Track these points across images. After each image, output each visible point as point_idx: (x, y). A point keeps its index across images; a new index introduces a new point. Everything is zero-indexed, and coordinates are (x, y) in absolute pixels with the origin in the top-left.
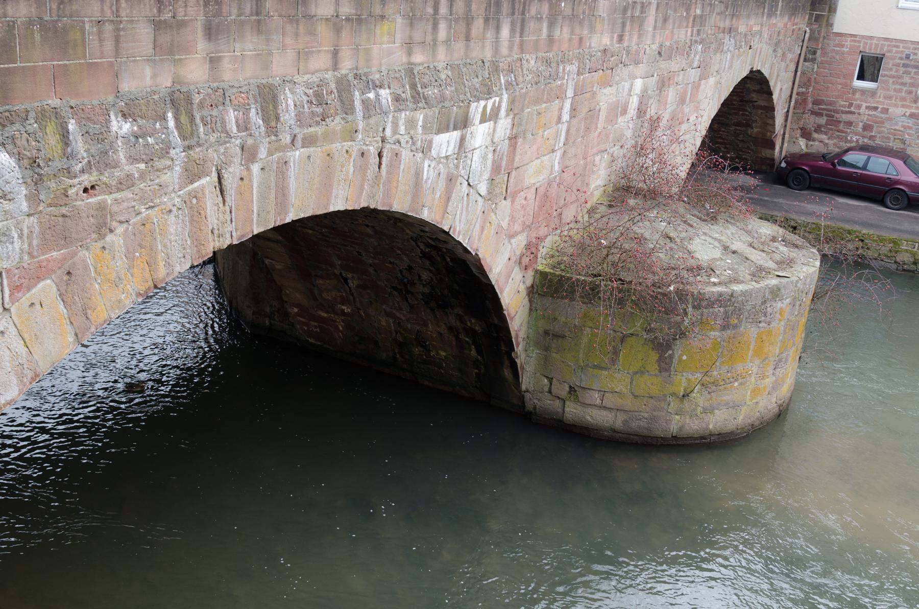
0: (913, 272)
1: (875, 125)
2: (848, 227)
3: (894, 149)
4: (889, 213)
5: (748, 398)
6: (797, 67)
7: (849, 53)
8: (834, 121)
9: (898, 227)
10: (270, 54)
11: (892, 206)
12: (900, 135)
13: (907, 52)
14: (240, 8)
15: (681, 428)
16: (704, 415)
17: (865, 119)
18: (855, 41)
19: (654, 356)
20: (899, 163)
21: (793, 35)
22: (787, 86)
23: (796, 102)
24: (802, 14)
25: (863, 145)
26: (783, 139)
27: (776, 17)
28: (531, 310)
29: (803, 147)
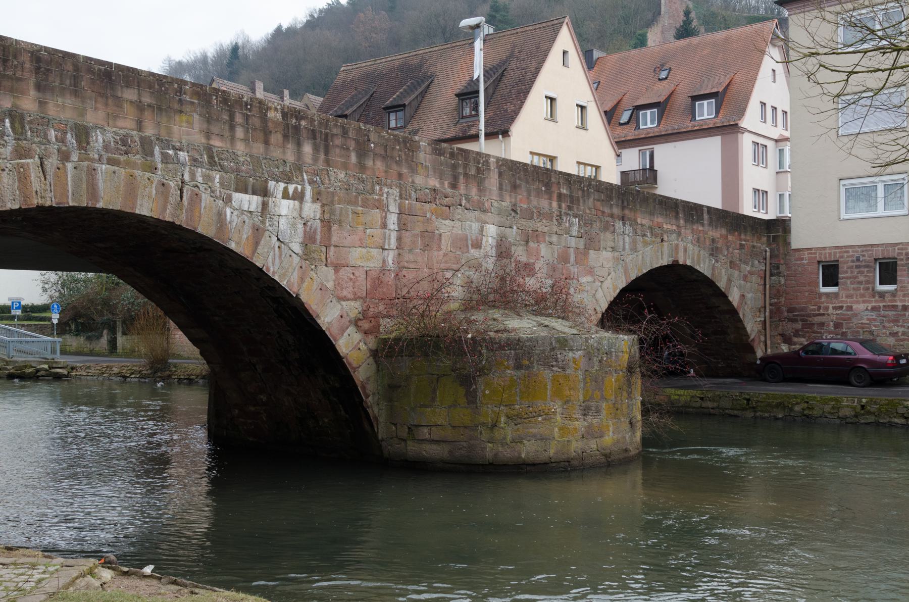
1: (844, 322)
6: (765, 282)
10: (85, 109)
12: (867, 328)
13: (856, 255)
14: (61, 80)
15: (496, 455)
16: (514, 444)
17: (834, 318)
18: (811, 253)
19: (462, 391)
23: (771, 311)
28: (378, 371)
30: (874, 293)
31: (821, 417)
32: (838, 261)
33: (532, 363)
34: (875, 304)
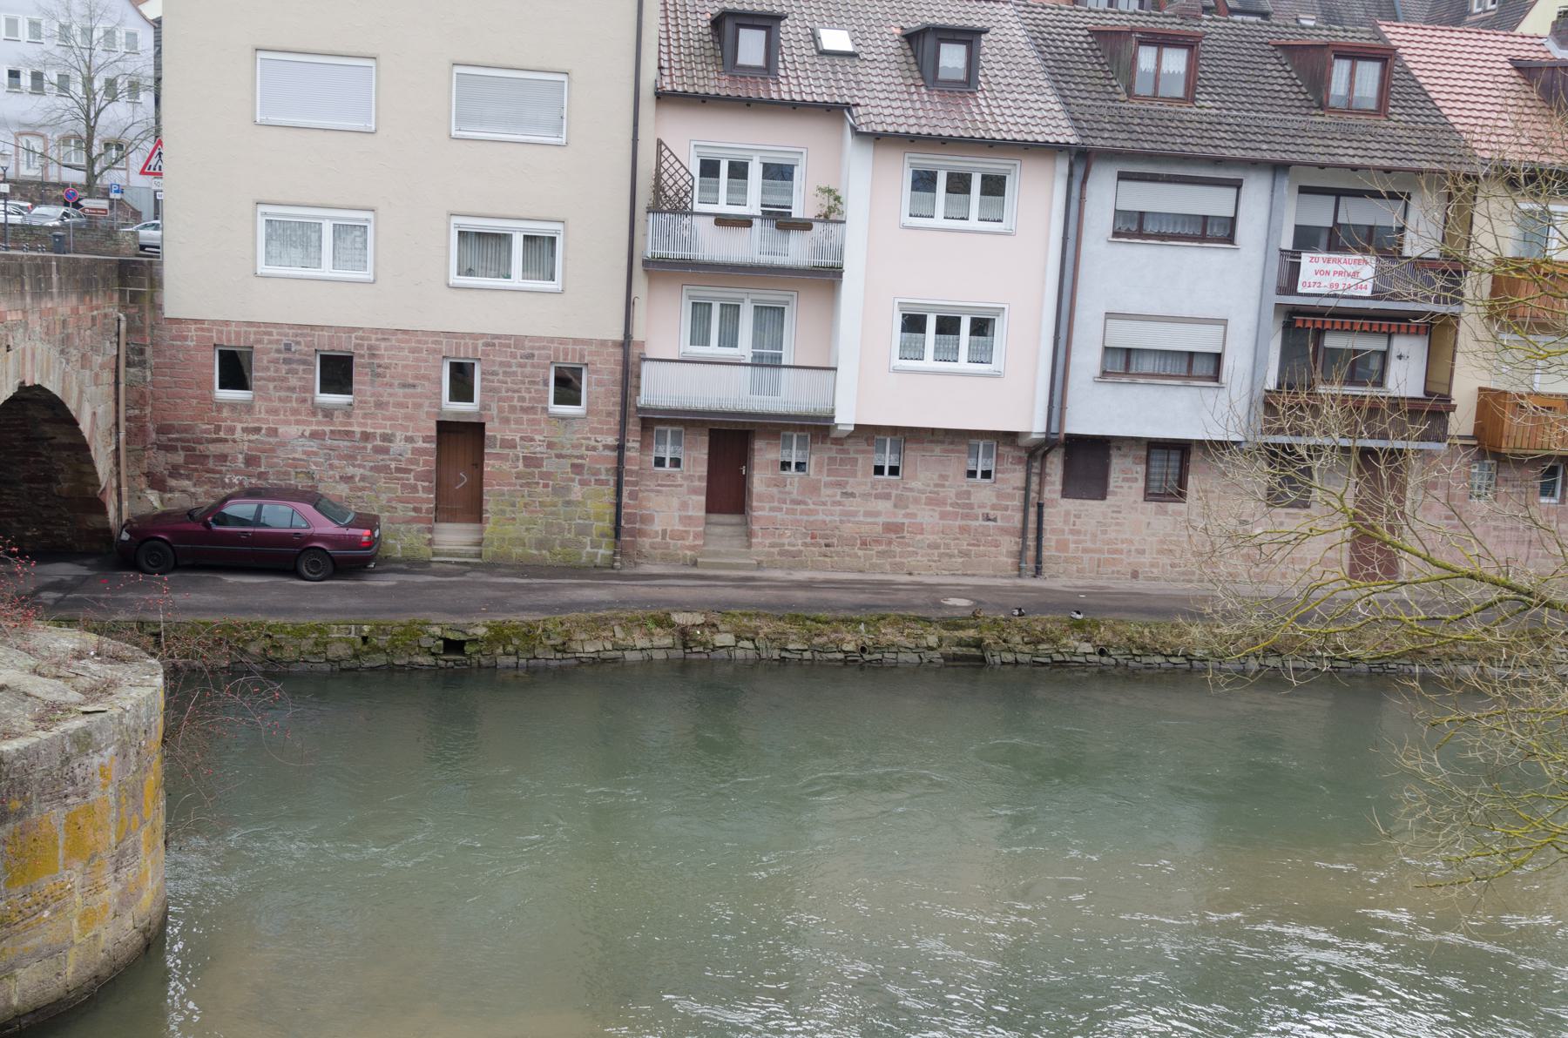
0: (355, 670)
1: (263, 456)
2: (188, 618)
3: (300, 488)
4: (308, 588)
5: (76, 932)
6: (117, 377)
7: (197, 348)
8: (196, 455)
9: (322, 606)
11: (311, 575)
12: (303, 467)
13: (285, 340)
17: (245, 448)
20: (307, 509)
21: (94, 325)
22: (105, 409)
23: (128, 432)
24: (105, 292)
25: (251, 489)
26: (119, 495)
27: (52, 299)
29: (157, 504)
30: (315, 409)
31: (297, 661)
32: (252, 347)
33: (28, 803)
34: (316, 428)
